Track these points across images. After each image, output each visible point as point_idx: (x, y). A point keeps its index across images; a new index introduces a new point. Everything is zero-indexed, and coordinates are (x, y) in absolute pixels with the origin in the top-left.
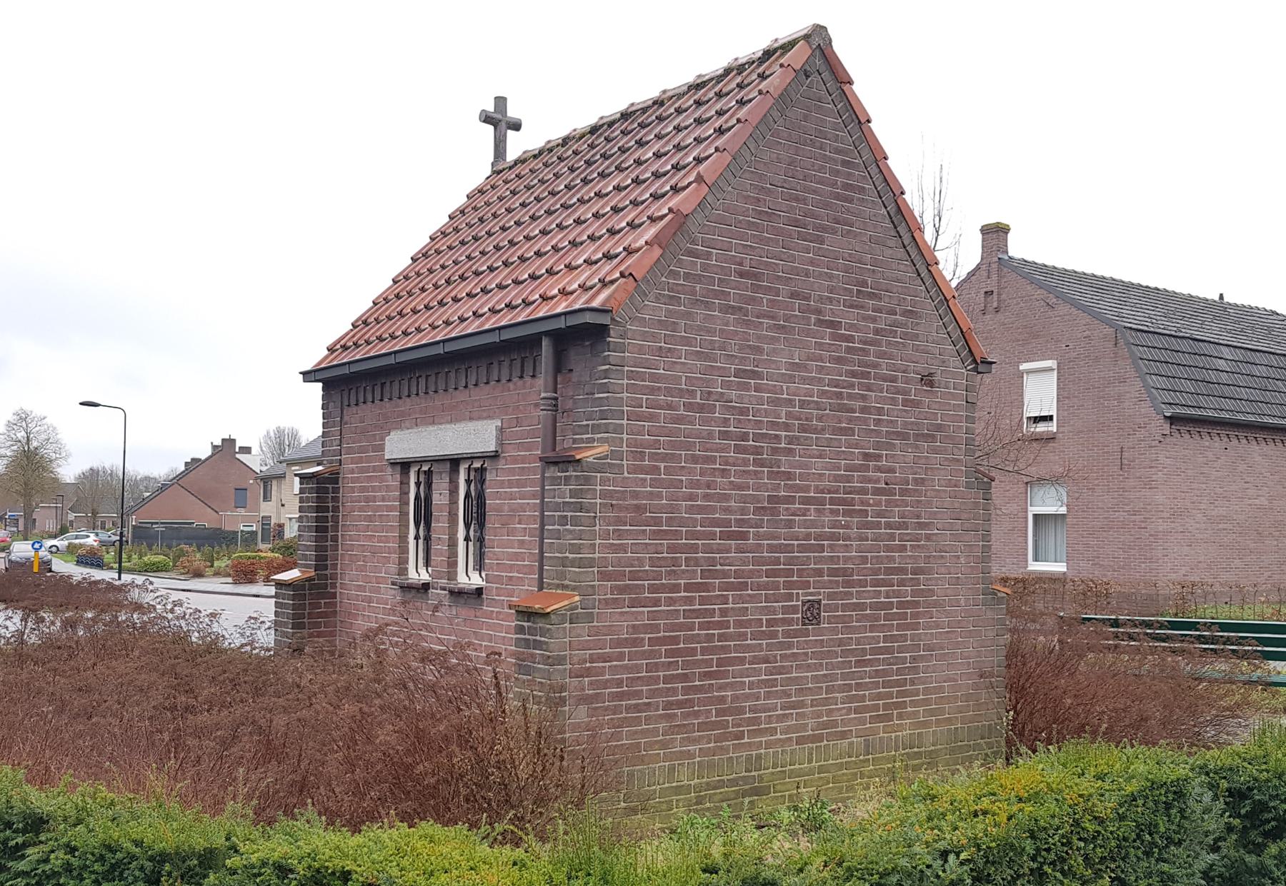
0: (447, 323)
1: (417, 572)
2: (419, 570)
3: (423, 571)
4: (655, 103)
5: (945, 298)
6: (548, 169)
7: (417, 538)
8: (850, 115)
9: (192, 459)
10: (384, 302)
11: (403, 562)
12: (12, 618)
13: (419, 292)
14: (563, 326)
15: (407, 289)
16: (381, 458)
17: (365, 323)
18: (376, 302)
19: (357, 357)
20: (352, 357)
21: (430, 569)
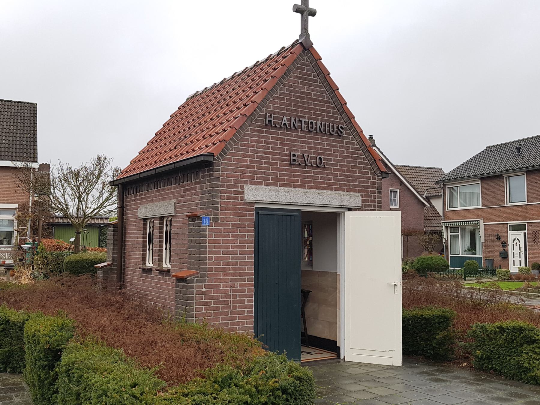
0: (134, 169)
1: (166, 264)
2: (167, 263)
3: (168, 264)
4: (242, 72)
5: (358, 133)
6: (249, 78)
7: (166, 249)
8: (317, 68)
9: (487, 147)
10: (213, 127)
11: (144, 259)
12: (187, 359)
13: (189, 136)
14: (138, 177)
15: (213, 124)
16: (242, 199)
17: (135, 162)
18: (140, 153)
19: (190, 157)
20: (175, 160)
21: (171, 263)
